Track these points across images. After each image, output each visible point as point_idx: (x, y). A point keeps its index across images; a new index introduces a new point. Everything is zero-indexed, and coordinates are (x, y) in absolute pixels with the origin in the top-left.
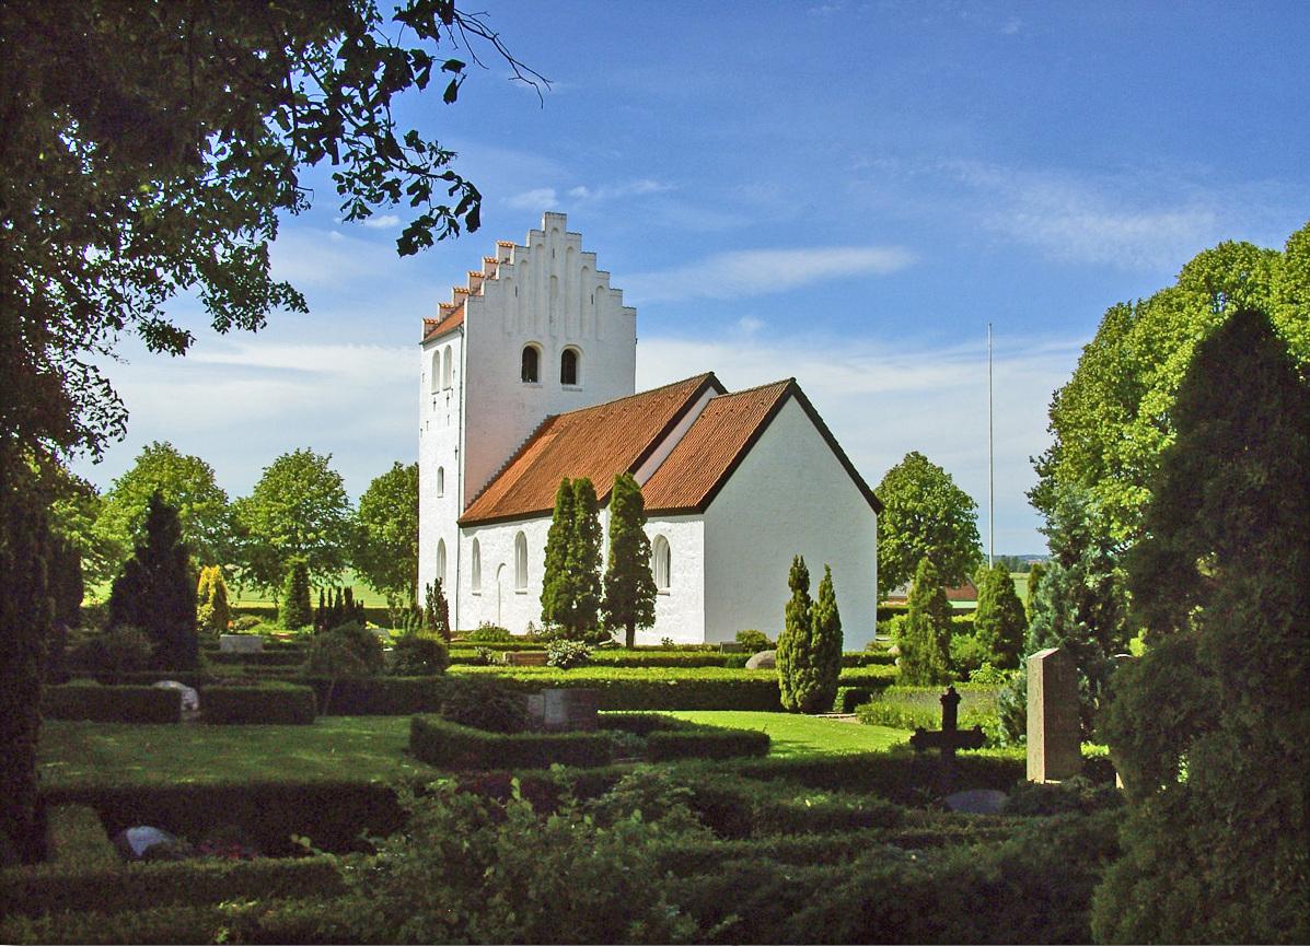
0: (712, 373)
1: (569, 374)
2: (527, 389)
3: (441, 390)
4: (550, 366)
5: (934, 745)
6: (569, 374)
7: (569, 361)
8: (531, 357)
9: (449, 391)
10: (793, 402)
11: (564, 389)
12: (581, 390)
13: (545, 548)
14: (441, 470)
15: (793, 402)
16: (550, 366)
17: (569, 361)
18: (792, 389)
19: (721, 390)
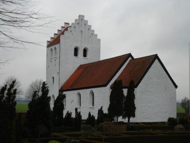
0: (157, 54)
1: (85, 55)
2: (75, 58)
3: (53, 58)
4: (81, 53)
5: (128, 93)
6: (85, 55)
7: (76, 54)
8: (76, 50)
9: (56, 59)
10: (157, 61)
11: (84, 58)
12: (88, 59)
13: (83, 16)
14: (53, 78)
15: (157, 61)
16: (81, 53)
17: (76, 54)
18: (156, 57)
19: (132, 57)
